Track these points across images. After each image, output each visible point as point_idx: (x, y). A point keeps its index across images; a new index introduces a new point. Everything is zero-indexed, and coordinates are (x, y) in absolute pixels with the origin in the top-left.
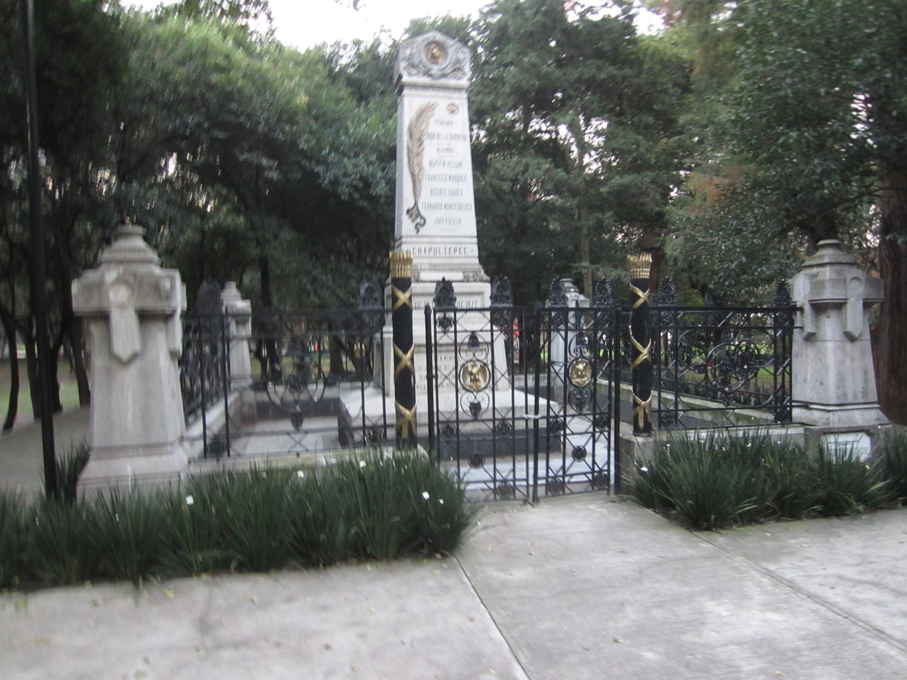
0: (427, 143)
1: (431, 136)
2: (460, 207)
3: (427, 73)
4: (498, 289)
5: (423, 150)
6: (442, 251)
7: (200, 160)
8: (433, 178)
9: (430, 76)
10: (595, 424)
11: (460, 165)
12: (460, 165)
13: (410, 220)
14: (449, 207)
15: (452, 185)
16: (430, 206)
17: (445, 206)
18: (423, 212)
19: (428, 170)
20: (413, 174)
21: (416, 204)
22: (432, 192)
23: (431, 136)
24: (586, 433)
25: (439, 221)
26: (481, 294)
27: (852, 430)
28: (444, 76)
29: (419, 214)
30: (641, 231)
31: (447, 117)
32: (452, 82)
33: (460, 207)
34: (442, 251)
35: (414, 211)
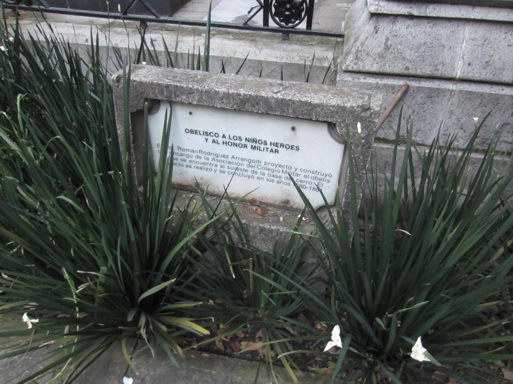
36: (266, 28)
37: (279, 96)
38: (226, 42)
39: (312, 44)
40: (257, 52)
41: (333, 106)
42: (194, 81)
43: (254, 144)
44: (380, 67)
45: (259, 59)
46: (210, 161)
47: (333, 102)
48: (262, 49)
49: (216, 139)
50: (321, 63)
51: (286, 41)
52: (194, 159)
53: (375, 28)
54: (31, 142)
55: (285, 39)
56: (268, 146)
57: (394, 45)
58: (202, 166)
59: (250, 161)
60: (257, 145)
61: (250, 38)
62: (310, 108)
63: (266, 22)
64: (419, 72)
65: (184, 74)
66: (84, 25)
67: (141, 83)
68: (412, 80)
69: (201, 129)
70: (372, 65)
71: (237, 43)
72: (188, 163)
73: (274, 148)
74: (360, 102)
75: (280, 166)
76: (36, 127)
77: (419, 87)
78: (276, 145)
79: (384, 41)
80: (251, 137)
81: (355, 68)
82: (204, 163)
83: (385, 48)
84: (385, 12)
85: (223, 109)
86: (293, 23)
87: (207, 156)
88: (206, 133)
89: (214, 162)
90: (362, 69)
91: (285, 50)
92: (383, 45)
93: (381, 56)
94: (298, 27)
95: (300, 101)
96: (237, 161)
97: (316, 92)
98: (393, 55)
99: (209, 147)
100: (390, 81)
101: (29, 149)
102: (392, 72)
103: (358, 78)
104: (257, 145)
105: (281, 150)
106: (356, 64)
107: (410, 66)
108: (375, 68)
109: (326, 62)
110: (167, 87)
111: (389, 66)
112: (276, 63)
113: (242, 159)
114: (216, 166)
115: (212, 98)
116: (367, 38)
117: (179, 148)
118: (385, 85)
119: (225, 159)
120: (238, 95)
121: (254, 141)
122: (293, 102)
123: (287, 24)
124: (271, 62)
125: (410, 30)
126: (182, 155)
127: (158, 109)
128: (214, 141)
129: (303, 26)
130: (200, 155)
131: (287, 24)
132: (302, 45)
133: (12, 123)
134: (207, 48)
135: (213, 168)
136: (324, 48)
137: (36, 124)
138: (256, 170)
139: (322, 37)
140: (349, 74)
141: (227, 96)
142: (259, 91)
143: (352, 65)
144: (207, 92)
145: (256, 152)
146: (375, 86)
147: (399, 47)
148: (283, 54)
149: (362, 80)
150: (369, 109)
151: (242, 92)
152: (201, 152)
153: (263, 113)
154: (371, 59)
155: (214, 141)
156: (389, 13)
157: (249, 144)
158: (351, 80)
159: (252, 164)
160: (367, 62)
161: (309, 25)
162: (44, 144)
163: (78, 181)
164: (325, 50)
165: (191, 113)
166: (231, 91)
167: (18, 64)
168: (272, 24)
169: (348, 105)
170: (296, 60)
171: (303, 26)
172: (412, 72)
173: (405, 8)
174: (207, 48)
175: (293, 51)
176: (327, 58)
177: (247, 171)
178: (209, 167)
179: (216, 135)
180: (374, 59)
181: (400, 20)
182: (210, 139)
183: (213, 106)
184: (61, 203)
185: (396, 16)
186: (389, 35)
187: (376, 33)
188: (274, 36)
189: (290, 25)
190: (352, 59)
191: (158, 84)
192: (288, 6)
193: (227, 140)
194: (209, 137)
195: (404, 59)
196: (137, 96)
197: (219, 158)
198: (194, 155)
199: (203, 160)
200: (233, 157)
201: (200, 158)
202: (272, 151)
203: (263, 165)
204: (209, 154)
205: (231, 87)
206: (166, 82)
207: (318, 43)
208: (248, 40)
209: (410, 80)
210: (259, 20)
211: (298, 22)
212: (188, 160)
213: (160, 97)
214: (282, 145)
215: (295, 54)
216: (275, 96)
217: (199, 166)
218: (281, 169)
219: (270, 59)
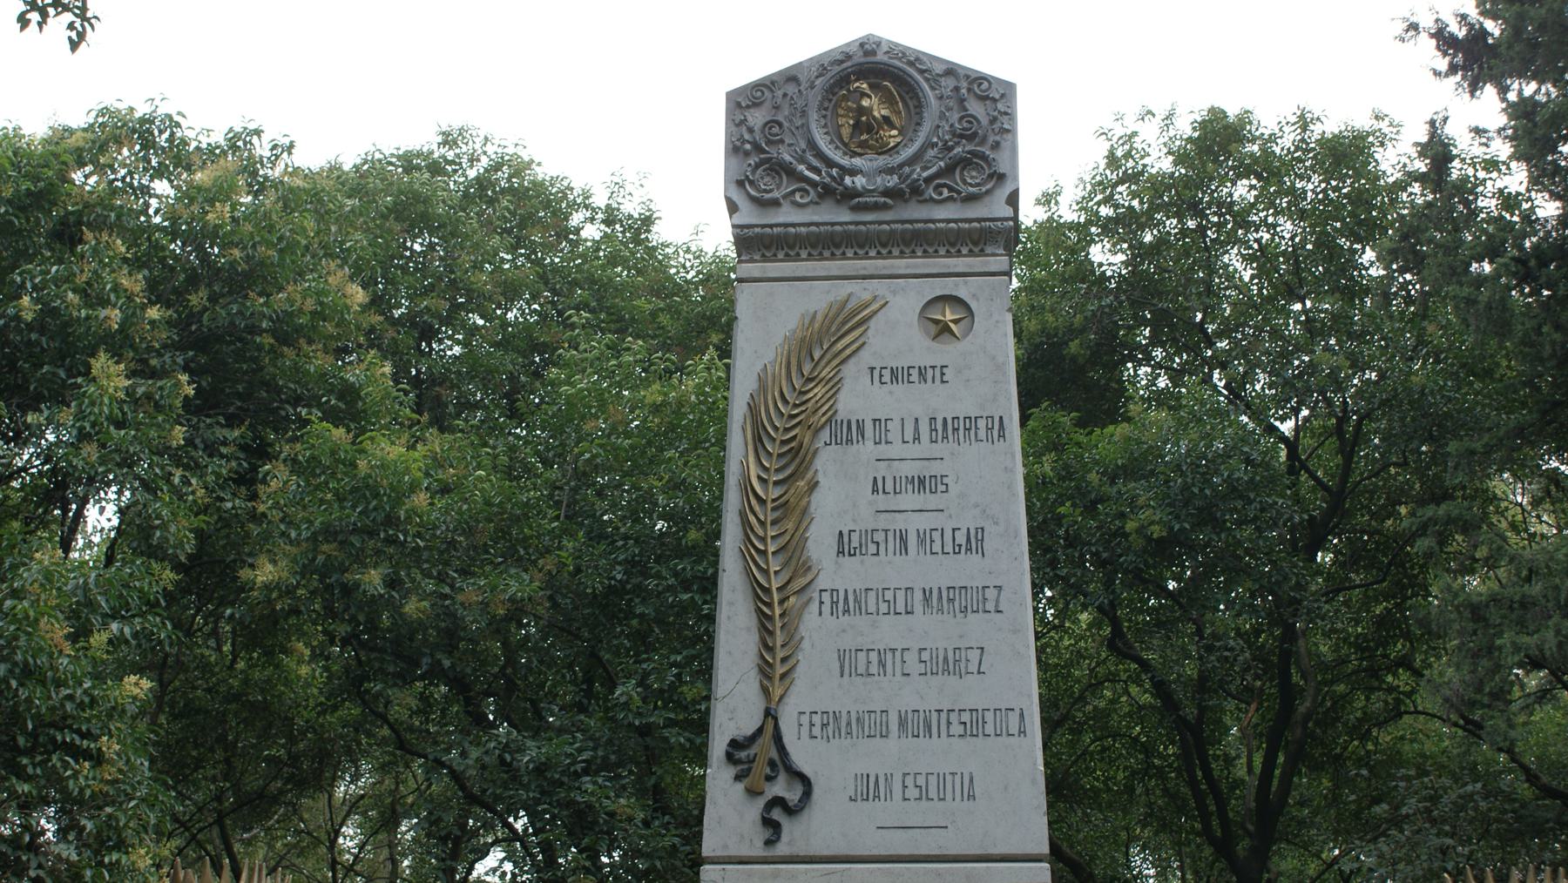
0: (827, 462)
1: (851, 432)
2: (974, 725)
3: (835, 193)
5: (813, 486)
7: (229, 497)
8: (845, 604)
9: (848, 197)
11: (974, 543)
14: (917, 725)
15: (937, 630)
16: (831, 724)
17: (902, 723)
18: (802, 754)
19: (832, 573)
20: (760, 594)
21: (770, 714)
22: (846, 663)
23: (851, 432)
25: (869, 789)
28: (911, 192)
29: (782, 763)
30: (643, 236)
31: (919, 348)
33: (974, 725)
35: (764, 749)
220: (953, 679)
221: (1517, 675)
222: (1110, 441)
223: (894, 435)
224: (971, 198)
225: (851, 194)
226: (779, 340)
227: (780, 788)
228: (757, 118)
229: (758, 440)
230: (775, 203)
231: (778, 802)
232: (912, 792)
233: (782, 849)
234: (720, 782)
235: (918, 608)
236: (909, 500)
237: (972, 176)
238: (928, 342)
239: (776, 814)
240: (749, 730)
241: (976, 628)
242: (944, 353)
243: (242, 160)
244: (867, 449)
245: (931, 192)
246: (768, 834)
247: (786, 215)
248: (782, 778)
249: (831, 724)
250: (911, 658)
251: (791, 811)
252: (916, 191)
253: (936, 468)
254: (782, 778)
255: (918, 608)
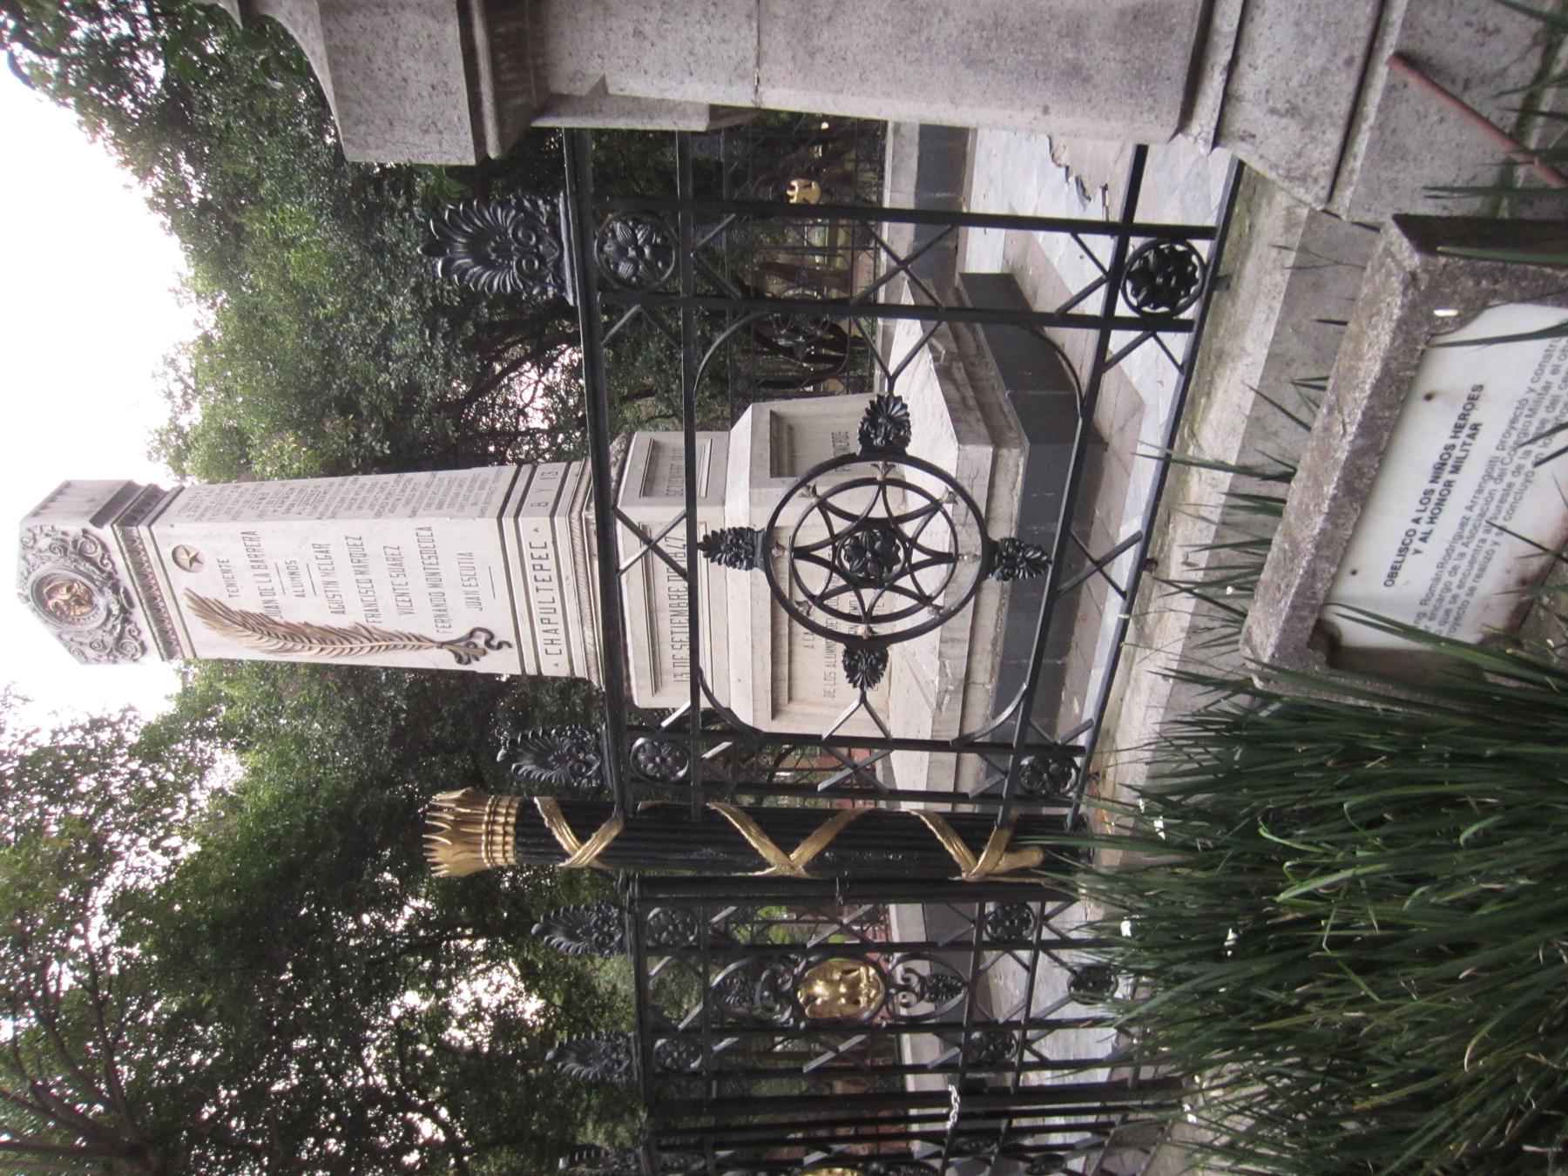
2: (429, 553)
4: (593, 870)
5: (306, 624)
6: (547, 596)
8: (372, 609)
10: (1008, 944)
11: (322, 550)
12: (322, 550)
13: (482, 659)
14: (434, 578)
15: (379, 571)
16: (441, 616)
17: (435, 586)
21: (442, 645)
22: (408, 611)
24: (1031, 969)
25: (475, 601)
26: (655, 447)
27: (1377, 45)
32: (120, 561)
34: (547, 596)
36: (1195, 327)
37: (1352, 429)
38: (1213, 416)
39: (1250, 227)
40: (1247, 360)
41: (1393, 340)
42: (1292, 561)
43: (1448, 468)
44: (1333, 124)
45: (1262, 359)
46: (1469, 551)
47: (1386, 339)
48: (1243, 349)
49: (1419, 535)
50: (1297, 224)
51: (1233, 283)
52: (1456, 580)
53: (1242, 139)
54: (1349, 847)
55: (1228, 287)
56: (1458, 442)
57: (1289, 96)
58: (1476, 567)
59: (1488, 476)
60: (1450, 463)
61: (1213, 362)
62: (1387, 381)
63: (1185, 326)
64: (1364, 33)
65: (1276, 569)
66: (1134, 673)
67: (1279, 647)
68: (1383, 42)
69: (1391, 557)
70: (1325, 145)
71: (1219, 395)
72: (1463, 593)
73: (1466, 431)
74: (1396, 284)
75: (1514, 421)
76: (1322, 827)
77: (1403, 25)
78: (1458, 428)
79: (1275, 118)
80: (1429, 472)
81: (1325, 182)
82: (1471, 563)
83: (1293, 116)
84: (1213, 124)
85: (1356, 526)
86: (1195, 268)
87: (1455, 555)
88: (1403, 550)
89: (1473, 545)
90: (1329, 168)
91: (1254, 298)
92: (1284, 121)
93: (1309, 123)
94: (1205, 257)
95: (1370, 397)
96: (1481, 501)
97: (1358, 355)
98: (1311, 98)
99: (1434, 550)
100: (1374, 97)
101: (1359, 854)
102: (1351, 98)
103: (1352, 171)
104: (1450, 463)
105: (1473, 418)
106: (1316, 180)
107: (1345, 54)
108: (1334, 137)
109: (1298, 210)
110: (1294, 607)
111: (1336, 104)
112: (1281, 323)
113: (1480, 491)
114: (1484, 541)
115: (1332, 540)
116: (1261, 157)
117: (1424, 602)
118: (1380, 110)
119: (1470, 524)
120: (1334, 498)
121: (1439, 468)
122: (1369, 408)
123: (1195, 281)
124: (1276, 334)
125: (1260, 62)
126: (1441, 600)
127: (1332, 624)
128: (1424, 540)
129: (1203, 247)
130: (1449, 567)
131: (1195, 281)
132: (1247, 251)
133: (1305, 860)
134: (1220, 466)
135: (1487, 546)
136: (1264, 202)
137: (1313, 825)
138: (1512, 467)
139: (1239, 198)
140: (1336, 193)
141: (1332, 516)
142: (1336, 461)
143: (1316, 189)
144: (1318, 547)
145: (1466, 466)
146: (1377, 133)
147: (1294, 83)
148: (1261, 306)
149: (1358, 164)
150: (1413, 275)
151: (1330, 490)
152: (1441, 566)
153: (1380, 462)
154: (1310, 147)
155: (1424, 540)
156: (1216, 115)
157: (1446, 476)
158: (1352, 189)
159: (1496, 473)
160: (1316, 155)
161: (1203, 233)
162: (1352, 829)
163: (1450, 800)
164: (1270, 203)
165: (1354, 573)
166: (1325, 508)
167: (1198, 812)
168: (1189, 314)
169: (1397, 313)
170: (1280, 279)
171: (1203, 247)
172: (1359, 50)
173: (1212, 79)
174: (1220, 466)
175: (1259, 282)
176: (1288, 208)
177: (1510, 485)
178: (1482, 555)
179: (1410, 534)
180: (1313, 139)
181: (1234, 86)
182: (1416, 544)
183: (1348, 541)
184: (1470, 844)
185: (1227, 97)
186: (1265, 108)
187: (1253, 136)
188: (1217, 306)
189: (1198, 274)
190: (1302, 190)
191: (1287, 621)
192: (1159, 280)
193: (1426, 516)
194: (1412, 548)
195: (1324, 71)
196: (1301, 659)
197: (1466, 533)
198: (1446, 577)
199: (1464, 564)
200: (1470, 508)
201: (1455, 569)
202: (1472, 436)
203: (1502, 454)
204: (1450, 551)
205: (1317, 505)
206: (1285, 605)
207: (1249, 211)
208: (1215, 368)
209: (1381, 48)
210: (1178, 343)
211: (1194, 259)
212: (1455, 591)
213: (1311, 623)
214: (1463, 417)
215: (1267, 280)
216: (1351, 438)
217: (1475, 571)
218: (1522, 420)
219: (1269, 334)
220: (405, 562)
221: (392, 902)
222: (454, 1023)
223: (269, 586)
224: (104, 547)
225: (123, 610)
226: (225, 640)
227: (480, 641)
228: (90, 653)
229: (288, 651)
230: (142, 645)
231: (488, 643)
232: (473, 582)
233: (513, 641)
234: (482, 666)
235: (366, 577)
236: (305, 579)
237: (90, 548)
238: (206, 568)
239: (495, 643)
240: (452, 656)
241: (372, 549)
242: (206, 556)
243: (230, 871)
244: (279, 599)
245: (109, 568)
246: (505, 647)
247: (147, 637)
248: (474, 640)
249: (441, 616)
250: (397, 581)
251: (492, 636)
252: (110, 576)
253: (282, 566)
254: (474, 640)
255: (366, 577)
